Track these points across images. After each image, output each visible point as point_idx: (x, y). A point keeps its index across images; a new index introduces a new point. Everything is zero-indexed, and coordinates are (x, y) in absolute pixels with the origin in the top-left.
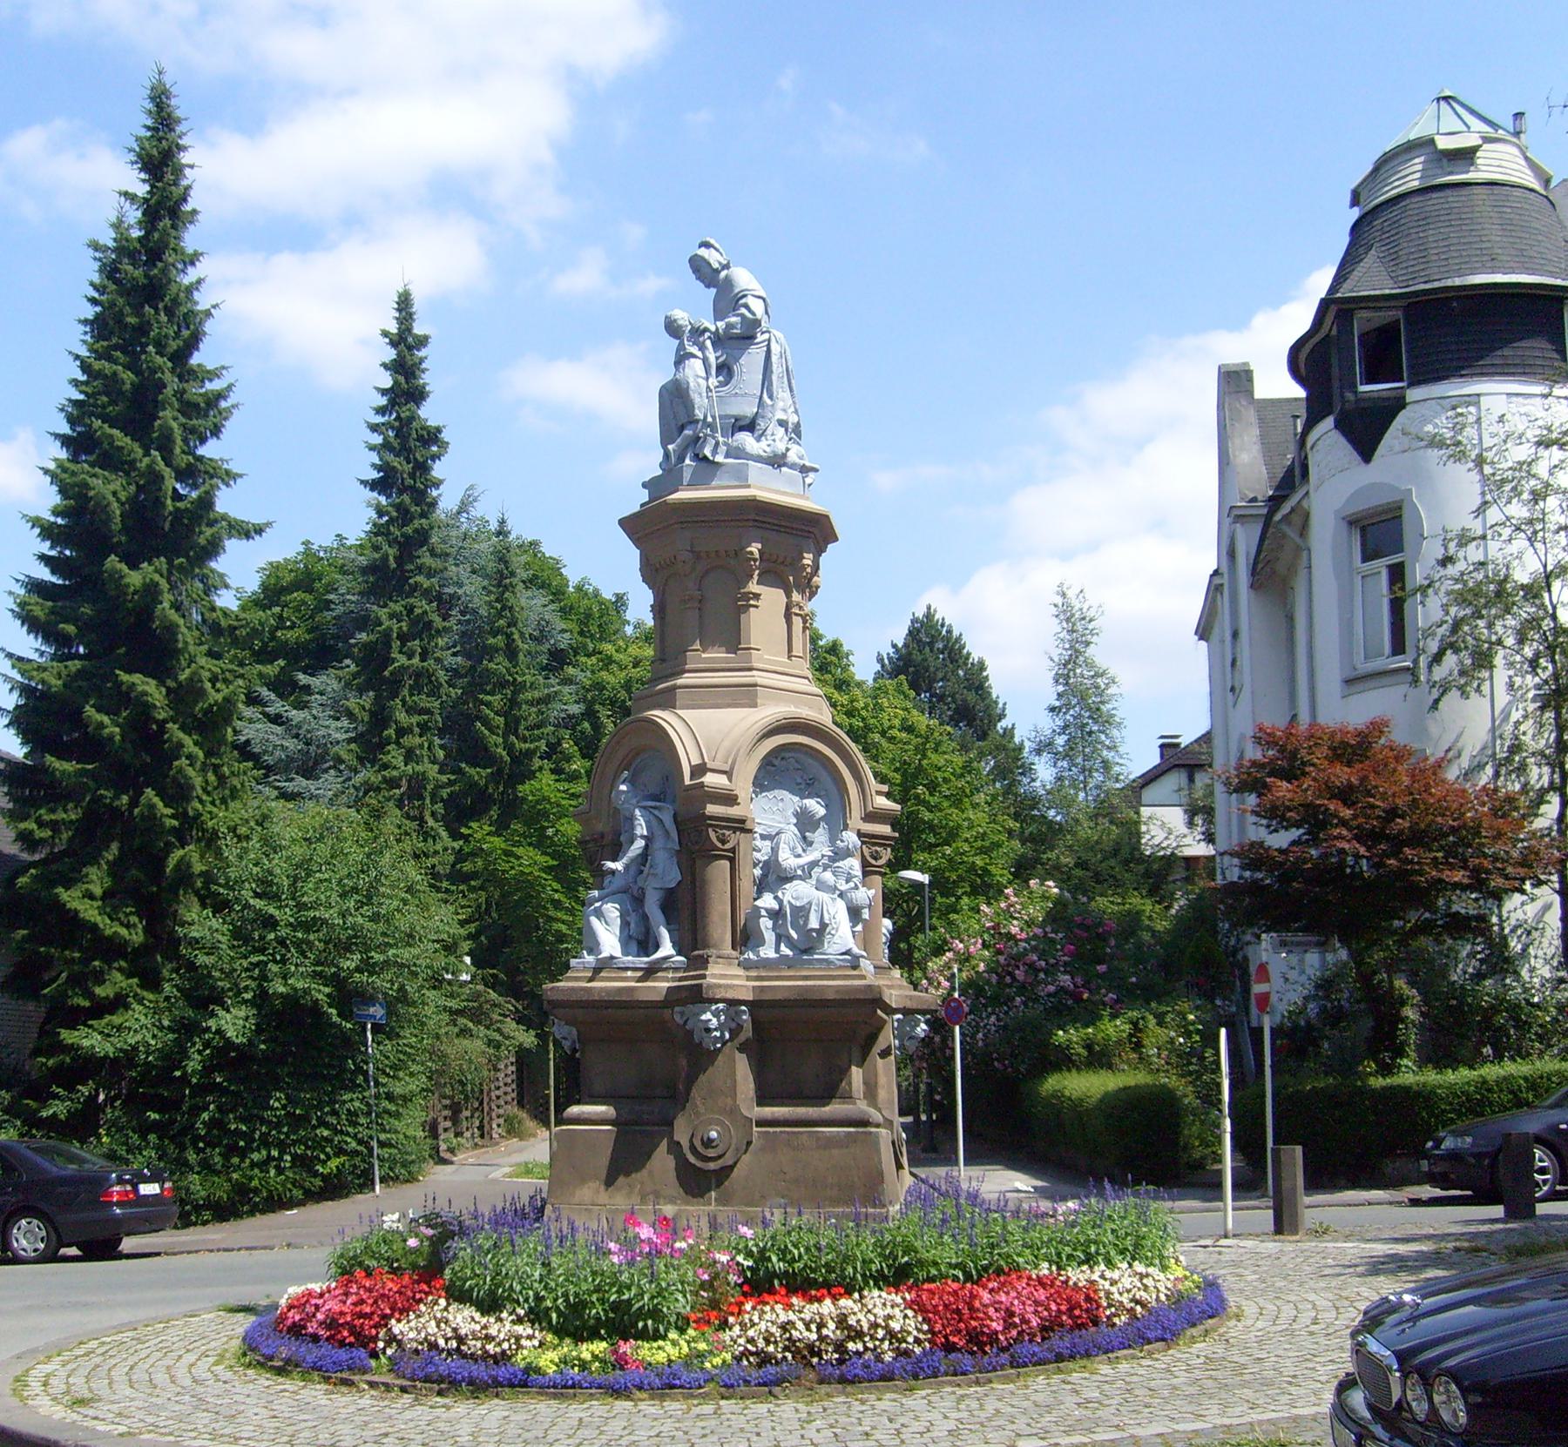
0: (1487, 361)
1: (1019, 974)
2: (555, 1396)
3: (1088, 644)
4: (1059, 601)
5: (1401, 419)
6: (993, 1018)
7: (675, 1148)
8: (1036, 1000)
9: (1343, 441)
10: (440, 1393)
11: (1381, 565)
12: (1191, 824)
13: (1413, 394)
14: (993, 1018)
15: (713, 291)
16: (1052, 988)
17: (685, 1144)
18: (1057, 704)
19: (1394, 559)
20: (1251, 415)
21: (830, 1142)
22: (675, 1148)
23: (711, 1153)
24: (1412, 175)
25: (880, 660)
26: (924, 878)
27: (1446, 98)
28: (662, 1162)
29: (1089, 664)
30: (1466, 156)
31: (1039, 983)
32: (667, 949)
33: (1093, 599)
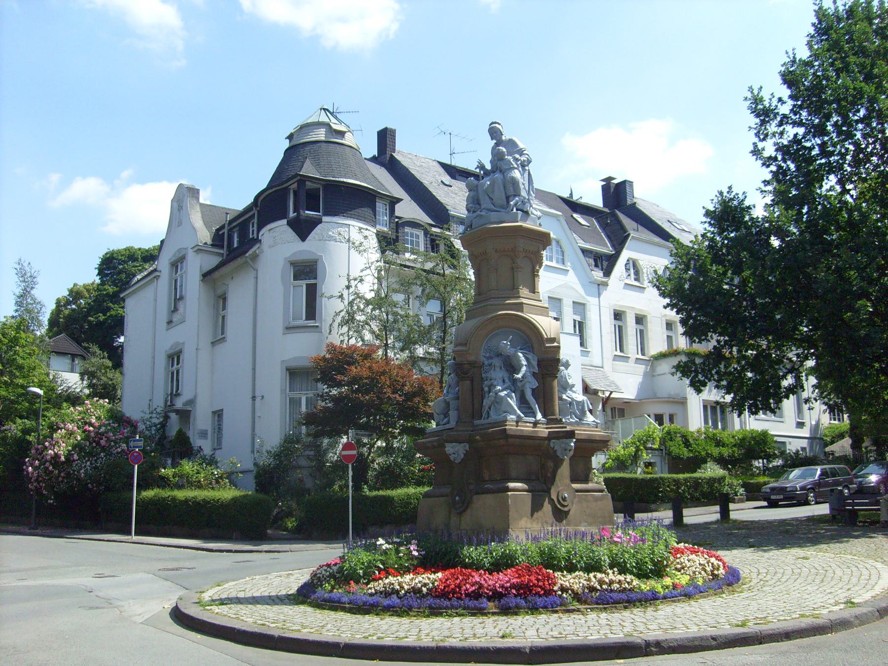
0: (352, 212)
1: (103, 442)
2: (674, 601)
3: (32, 288)
4: (18, 267)
5: (319, 226)
6: (88, 463)
7: (551, 501)
8: (110, 455)
9: (290, 230)
10: (626, 608)
11: (303, 283)
12: (82, 379)
13: (325, 219)
14: (88, 463)
15: (495, 141)
16: (119, 450)
17: (555, 500)
18: (15, 314)
19: (312, 281)
20: (198, 208)
21: (596, 499)
22: (551, 501)
23: (565, 504)
24: (320, 135)
25: (75, 285)
26: (41, 392)
27: (324, 109)
28: (547, 507)
29: (34, 299)
30: (341, 134)
31: (112, 447)
32: (539, 416)
33: (35, 266)
